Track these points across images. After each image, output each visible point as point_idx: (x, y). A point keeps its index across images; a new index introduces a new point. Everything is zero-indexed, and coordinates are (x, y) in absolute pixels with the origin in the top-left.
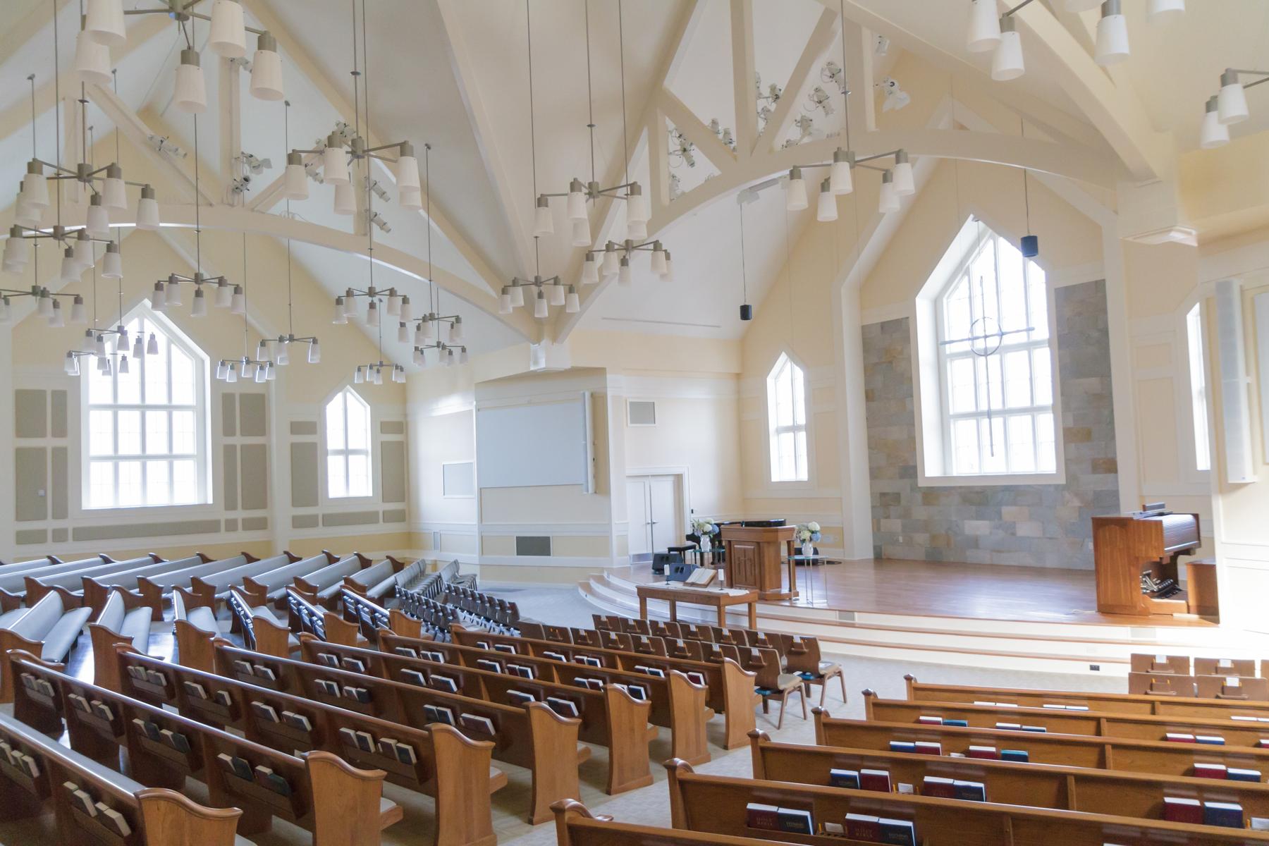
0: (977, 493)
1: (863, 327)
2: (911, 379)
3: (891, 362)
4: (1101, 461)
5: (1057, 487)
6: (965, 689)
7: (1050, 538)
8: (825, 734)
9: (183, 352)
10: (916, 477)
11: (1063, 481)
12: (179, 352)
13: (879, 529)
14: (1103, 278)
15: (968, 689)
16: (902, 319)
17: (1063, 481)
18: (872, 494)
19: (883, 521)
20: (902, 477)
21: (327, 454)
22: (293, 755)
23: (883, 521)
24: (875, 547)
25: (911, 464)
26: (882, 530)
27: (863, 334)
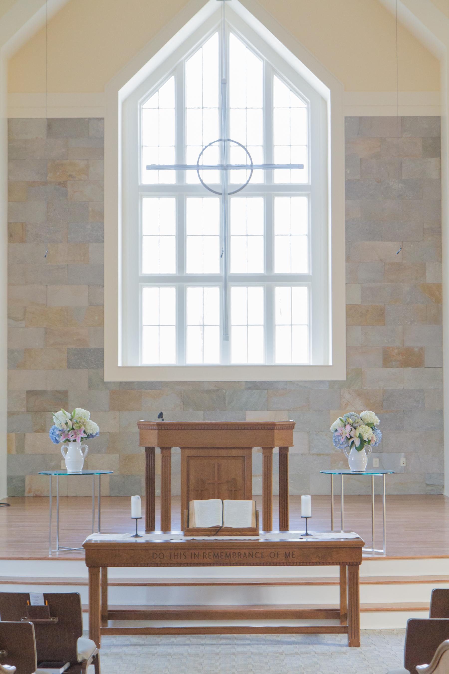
0: (208, 392)
1: (9, 121)
2: (101, 215)
3: (64, 184)
4: (396, 351)
5: (332, 383)
6: (371, 612)
7: (319, 455)
8: (327, 644)
9: (248, 47)
10: (102, 365)
11: (341, 376)
12: (242, 46)
13: (20, 449)
14: (439, 115)
15: (369, 612)
16: (90, 119)
17: (341, 376)
18: (10, 393)
19: (30, 438)
20: (71, 365)
21: (203, 198)
22: (21, 621)
23: (30, 438)
24: (10, 479)
25: (93, 346)
26: (28, 450)
27: (10, 131)
